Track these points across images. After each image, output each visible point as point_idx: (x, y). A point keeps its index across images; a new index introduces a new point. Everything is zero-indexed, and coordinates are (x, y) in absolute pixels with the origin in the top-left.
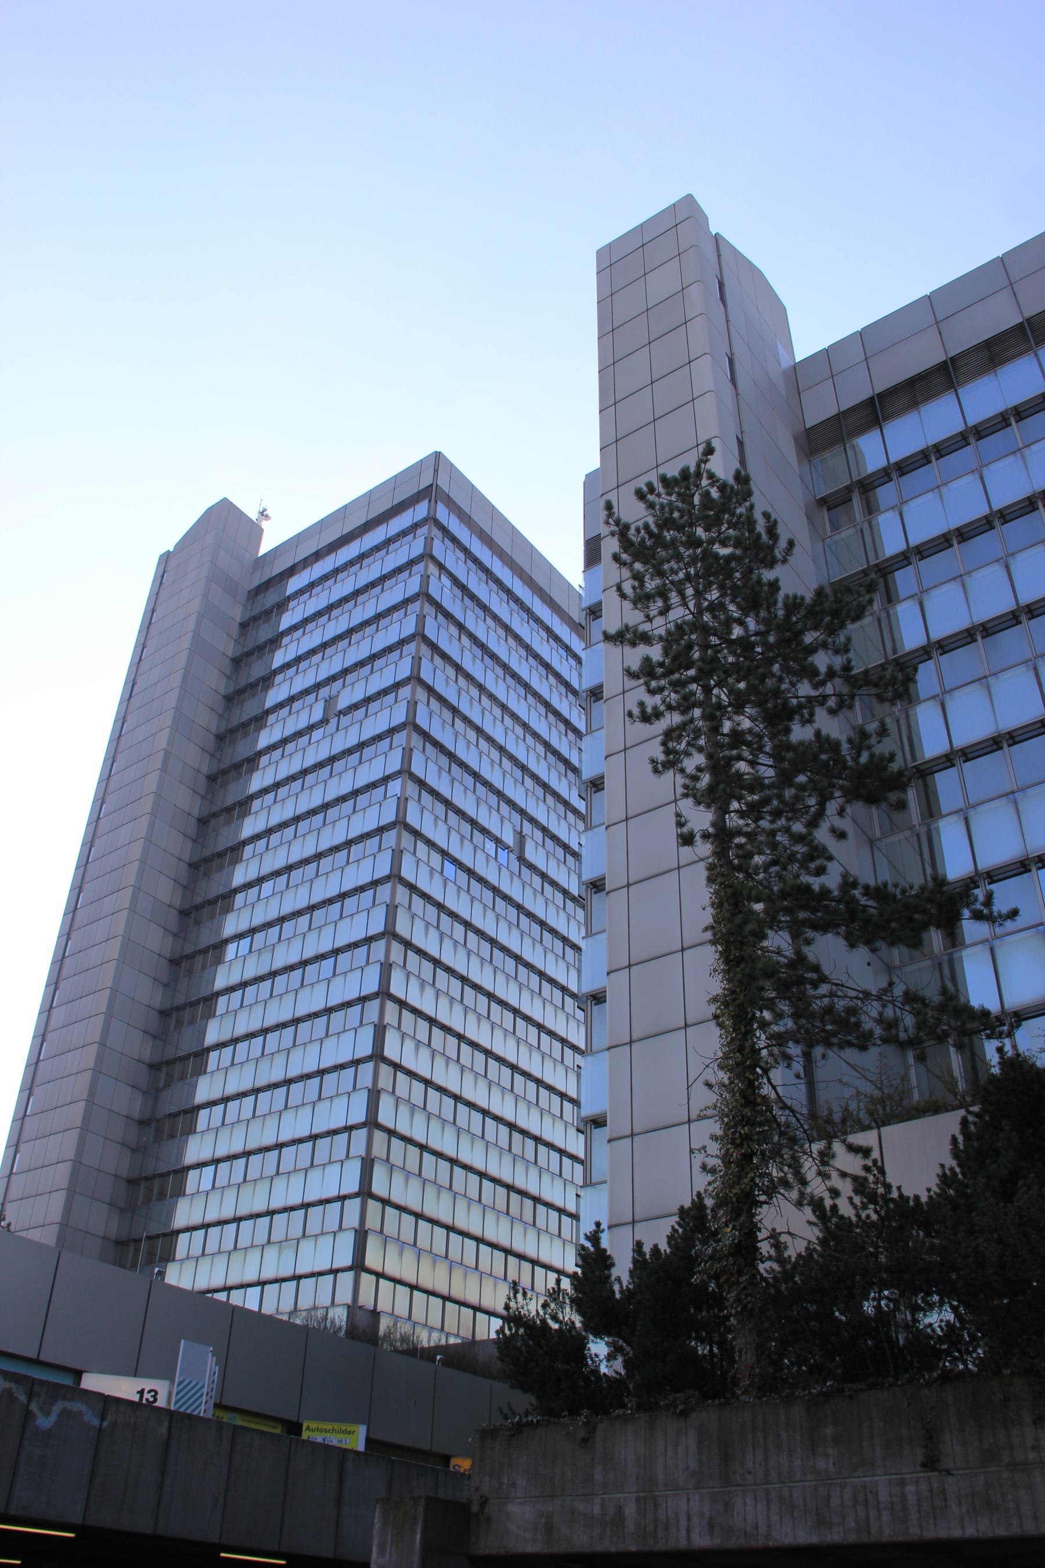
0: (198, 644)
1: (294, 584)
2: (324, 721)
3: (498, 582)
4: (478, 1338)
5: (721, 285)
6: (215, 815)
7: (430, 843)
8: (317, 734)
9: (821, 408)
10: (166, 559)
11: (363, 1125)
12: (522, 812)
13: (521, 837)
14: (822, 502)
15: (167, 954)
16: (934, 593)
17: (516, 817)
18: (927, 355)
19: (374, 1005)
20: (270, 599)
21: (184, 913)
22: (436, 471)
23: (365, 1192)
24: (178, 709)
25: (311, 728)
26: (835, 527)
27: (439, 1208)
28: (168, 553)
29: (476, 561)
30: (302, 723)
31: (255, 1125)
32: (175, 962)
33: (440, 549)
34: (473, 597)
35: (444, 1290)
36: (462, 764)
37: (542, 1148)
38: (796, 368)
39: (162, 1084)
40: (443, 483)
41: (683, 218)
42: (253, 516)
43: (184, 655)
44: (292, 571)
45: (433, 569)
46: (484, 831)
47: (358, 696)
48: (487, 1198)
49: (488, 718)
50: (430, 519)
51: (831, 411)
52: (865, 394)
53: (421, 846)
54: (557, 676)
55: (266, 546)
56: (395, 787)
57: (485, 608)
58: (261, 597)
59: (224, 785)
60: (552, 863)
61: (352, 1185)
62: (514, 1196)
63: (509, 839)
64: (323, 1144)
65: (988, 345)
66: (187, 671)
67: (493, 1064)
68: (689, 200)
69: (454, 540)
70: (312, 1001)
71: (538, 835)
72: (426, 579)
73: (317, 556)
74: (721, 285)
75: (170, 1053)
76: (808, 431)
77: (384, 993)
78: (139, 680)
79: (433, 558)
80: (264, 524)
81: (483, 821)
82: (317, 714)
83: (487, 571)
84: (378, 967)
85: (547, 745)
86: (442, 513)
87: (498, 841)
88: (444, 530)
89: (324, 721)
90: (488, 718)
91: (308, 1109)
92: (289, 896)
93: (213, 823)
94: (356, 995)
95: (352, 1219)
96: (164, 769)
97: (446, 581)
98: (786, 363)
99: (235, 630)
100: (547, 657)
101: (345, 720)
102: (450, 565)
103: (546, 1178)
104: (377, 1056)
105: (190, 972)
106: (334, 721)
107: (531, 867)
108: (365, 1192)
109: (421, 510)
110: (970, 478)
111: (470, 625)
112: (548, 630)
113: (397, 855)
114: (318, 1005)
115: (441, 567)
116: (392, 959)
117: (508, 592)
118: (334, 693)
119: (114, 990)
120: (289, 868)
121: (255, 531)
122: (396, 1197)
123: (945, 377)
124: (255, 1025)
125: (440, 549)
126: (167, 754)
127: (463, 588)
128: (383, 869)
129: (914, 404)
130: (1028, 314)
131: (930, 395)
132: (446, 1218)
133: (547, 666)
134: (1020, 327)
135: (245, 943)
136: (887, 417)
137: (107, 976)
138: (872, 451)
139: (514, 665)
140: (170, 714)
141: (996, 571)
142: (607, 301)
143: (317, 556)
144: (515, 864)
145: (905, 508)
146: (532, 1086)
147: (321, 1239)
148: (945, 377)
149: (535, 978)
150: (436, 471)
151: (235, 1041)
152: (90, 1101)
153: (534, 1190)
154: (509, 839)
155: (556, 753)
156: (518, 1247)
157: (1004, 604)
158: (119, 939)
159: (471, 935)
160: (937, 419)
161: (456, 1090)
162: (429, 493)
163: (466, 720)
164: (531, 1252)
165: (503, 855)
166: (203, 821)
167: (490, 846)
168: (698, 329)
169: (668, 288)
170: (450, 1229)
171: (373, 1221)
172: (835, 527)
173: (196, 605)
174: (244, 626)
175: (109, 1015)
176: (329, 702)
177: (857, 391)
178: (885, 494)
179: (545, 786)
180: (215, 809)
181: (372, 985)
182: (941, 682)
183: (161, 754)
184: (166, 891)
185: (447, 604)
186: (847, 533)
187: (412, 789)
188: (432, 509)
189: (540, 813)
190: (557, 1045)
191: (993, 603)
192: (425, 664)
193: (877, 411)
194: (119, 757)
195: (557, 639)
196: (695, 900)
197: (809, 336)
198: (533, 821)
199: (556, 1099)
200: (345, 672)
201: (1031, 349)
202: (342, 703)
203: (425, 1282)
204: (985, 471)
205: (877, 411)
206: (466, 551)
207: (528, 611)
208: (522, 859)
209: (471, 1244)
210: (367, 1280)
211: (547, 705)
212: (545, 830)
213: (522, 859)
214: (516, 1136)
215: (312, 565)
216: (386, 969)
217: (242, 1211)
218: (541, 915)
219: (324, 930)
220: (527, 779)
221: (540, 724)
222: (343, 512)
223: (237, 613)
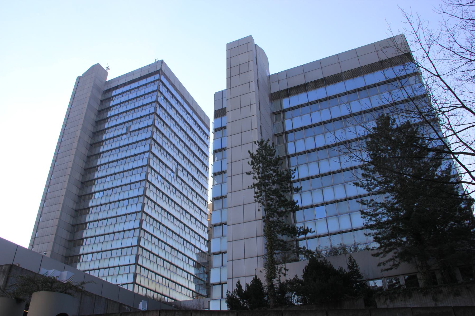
0: (89, 107)
1: (114, 93)
2: (126, 133)
3: (175, 98)
4: (139, 293)
5: (256, 59)
6: (92, 156)
7: (155, 171)
8: (124, 137)
9: (275, 89)
10: (79, 78)
11: (136, 246)
12: (178, 163)
13: (177, 169)
14: (274, 113)
15: (77, 194)
16: (298, 141)
17: (176, 164)
18: (300, 81)
19: (139, 214)
20: (109, 95)
21: (83, 183)
22: (162, 66)
23: (136, 263)
24: (83, 125)
25: (122, 135)
26: (277, 120)
27: (154, 268)
28: (80, 77)
29: (170, 92)
30: (120, 133)
31: (105, 244)
32: (80, 197)
33: (162, 89)
34: (169, 102)
35: (154, 289)
36: (164, 149)
37: (179, 253)
38: (270, 76)
39: (76, 230)
40: (163, 69)
41: (248, 41)
42: (105, 68)
43: (85, 109)
44: (117, 88)
45: (159, 94)
46: (168, 168)
47: (137, 128)
48: (158, 262)
49: (165, 131)
50: (159, 80)
51: (277, 90)
52: (286, 87)
53: (153, 172)
54: (189, 124)
55: (108, 79)
56: (147, 155)
57: (172, 105)
58: (107, 94)
59: (95, 147)
60: (185, 176)
61: (133, 261)
62: (171, 265)
63: (174, 170)
64: (125, 250)
65: (315, 82)
66: (86, 113)
67: (180, 238)
68: (251, 36)
69: (165, 86)
70: (122, 211)
71: (181, 169)
72: (157, 97)
73: (125, 84)
74: (256, 59)
75: (78, 222)
76: (272, 94)
77: (142, 211)
78: (71, 114)
79: (159, 91)
80: (108, 71)
81: (168, 165)
82: (124, 131)
83: (173, 95)
84: (141, 204)
85: (185, 144)
86: (163, 78)
87: (171, 170)
88: (163, 83)
89: (126, 133)
90: (165, 131)
91: (120, 241)
92: (115, 182)
93: (91, 158)
94: (135, 211)
95: (133, 270)
96: (79, 142)
97: (162, 97)
98: (268, 75)
99: (99, 102)
100: (186, 119)
101: (132, 134)
102: (164, 93)
103: (179, 261)
104: (140, 228)
105: (84, 200)
106: (129, 134)
107: (179, 178)
108: (136, 263)
109: (157, 77)
110: (308, 115)
111: (168, 110)
112: (187, 111)
113: (147, 174)
114: (123, 213)
115: (161, 93)
116: (145, 202)
117: (178, 100)
118: (129, 125)
119: (63, 204)
120: (115, 174)
121: (106, 74)
122: (144, 265)
123: (304, 88)
124: (105, 216)
125: (162, 89)
126: (80, 137)
127: (167, 99)
128: (143, 177)
129: (297, 93)
130: (325, 76)
131: (301, 92)
132: (162, 274)
133: (186, 122)
134: (322, 79)
135: (102, 193)
136: (290, 95)
137: (62, 199)
138: (286, 103)
139: (178, 122)
140: (81, 126)
141: (312, 139)
142: (229, 59)
143: (125, 84)
144: (175, 177)
145: (293, 119)
146: (158, 224)
147: (124, 275)
148: (304, 88)
149: (161, 194)
150: (162, 66)
151: (98, 220)
152: (56, 235)
153: (176, 264)
154: (174, 170)
155: (187, 146)
156: (172, 279)
157: (313, 147)
158: (65, 190)
159: (151, 186)
160: (301, 99)
161: (172, 245)
162: (159, 72)
163: (165, 137)
164: (175, 281)
165: (172, 174)
166: (88, 157)
167: (170, 172)
168: (252, 73)
169: (244, 56)
170: (156, 273)
171: (138, 271)
172: (277, 120)
173: (89, 94)
174: (102, 101)
175: (62, 211)
176: (128, 128)
177: (284, 86)
178: (288, 114)
179: (184, 155)
180: (93, 154)
181: (139, 209)
182: (298, 162)
183: (78, 137)
184: (78, 176)
185: (162, 104)
186: (279, 122)
187: (151, 156)
188: (160, 77)
189: (182, 162)
190: (166, 213)
191: (311, 146)
192: (156, 121)
193: (288, 92)
194: (64, 136)
195: (189, 114)
196: (260, 227)
197: (274, 69)
198: (180, 165)
199: (171, 233)
200: (133, 120)
201: (324, 86)
202: (132, 129)
203: (150, 287)
204: (312, 114)
205: (288, 92)
206: (168, 89)
207: (182, 106)
208: (177, 175)
209: (146, 271)
210: (136, 286)
211: (185, 133)
212: (183, 167)
213: (177, 175)
214: (173, 250)
215: (123, 87)
216: (143, 205)
217: (101, 267)
218: (158, 171)
219: (125, 192)
220: (174, 148)
221: (183, 138)
222: (133, 73)
223: (100, 97)
